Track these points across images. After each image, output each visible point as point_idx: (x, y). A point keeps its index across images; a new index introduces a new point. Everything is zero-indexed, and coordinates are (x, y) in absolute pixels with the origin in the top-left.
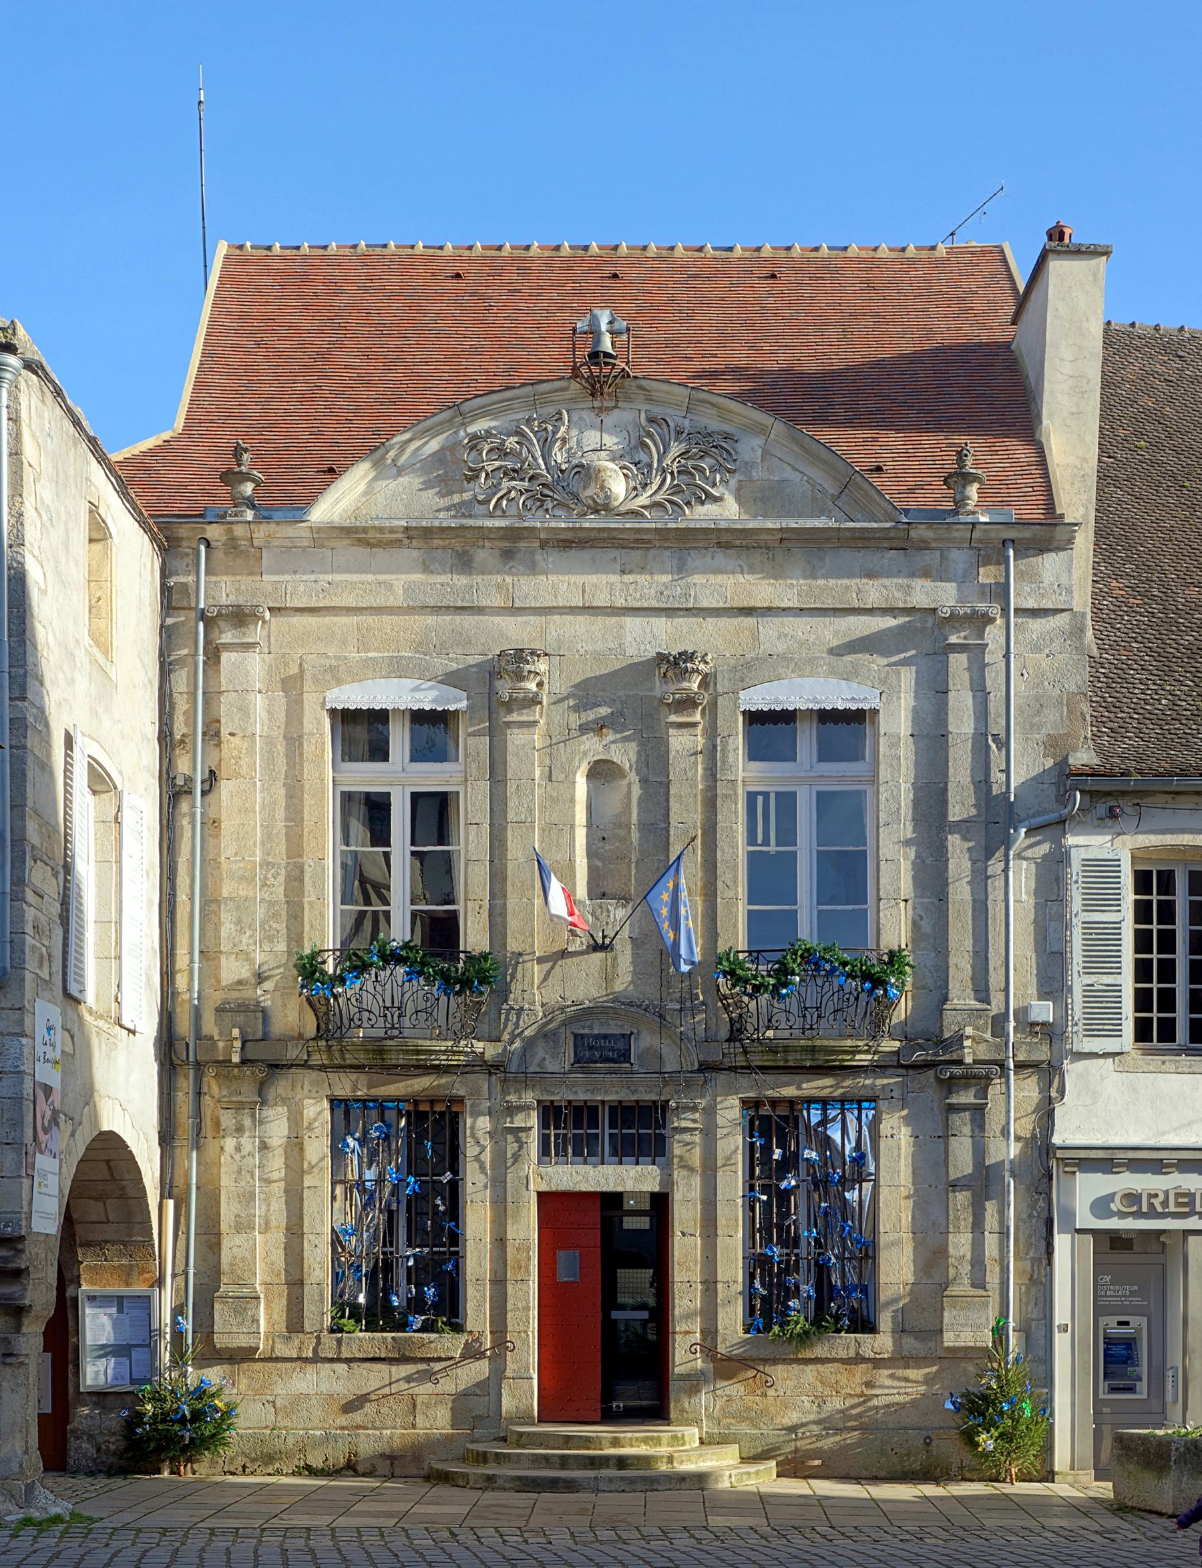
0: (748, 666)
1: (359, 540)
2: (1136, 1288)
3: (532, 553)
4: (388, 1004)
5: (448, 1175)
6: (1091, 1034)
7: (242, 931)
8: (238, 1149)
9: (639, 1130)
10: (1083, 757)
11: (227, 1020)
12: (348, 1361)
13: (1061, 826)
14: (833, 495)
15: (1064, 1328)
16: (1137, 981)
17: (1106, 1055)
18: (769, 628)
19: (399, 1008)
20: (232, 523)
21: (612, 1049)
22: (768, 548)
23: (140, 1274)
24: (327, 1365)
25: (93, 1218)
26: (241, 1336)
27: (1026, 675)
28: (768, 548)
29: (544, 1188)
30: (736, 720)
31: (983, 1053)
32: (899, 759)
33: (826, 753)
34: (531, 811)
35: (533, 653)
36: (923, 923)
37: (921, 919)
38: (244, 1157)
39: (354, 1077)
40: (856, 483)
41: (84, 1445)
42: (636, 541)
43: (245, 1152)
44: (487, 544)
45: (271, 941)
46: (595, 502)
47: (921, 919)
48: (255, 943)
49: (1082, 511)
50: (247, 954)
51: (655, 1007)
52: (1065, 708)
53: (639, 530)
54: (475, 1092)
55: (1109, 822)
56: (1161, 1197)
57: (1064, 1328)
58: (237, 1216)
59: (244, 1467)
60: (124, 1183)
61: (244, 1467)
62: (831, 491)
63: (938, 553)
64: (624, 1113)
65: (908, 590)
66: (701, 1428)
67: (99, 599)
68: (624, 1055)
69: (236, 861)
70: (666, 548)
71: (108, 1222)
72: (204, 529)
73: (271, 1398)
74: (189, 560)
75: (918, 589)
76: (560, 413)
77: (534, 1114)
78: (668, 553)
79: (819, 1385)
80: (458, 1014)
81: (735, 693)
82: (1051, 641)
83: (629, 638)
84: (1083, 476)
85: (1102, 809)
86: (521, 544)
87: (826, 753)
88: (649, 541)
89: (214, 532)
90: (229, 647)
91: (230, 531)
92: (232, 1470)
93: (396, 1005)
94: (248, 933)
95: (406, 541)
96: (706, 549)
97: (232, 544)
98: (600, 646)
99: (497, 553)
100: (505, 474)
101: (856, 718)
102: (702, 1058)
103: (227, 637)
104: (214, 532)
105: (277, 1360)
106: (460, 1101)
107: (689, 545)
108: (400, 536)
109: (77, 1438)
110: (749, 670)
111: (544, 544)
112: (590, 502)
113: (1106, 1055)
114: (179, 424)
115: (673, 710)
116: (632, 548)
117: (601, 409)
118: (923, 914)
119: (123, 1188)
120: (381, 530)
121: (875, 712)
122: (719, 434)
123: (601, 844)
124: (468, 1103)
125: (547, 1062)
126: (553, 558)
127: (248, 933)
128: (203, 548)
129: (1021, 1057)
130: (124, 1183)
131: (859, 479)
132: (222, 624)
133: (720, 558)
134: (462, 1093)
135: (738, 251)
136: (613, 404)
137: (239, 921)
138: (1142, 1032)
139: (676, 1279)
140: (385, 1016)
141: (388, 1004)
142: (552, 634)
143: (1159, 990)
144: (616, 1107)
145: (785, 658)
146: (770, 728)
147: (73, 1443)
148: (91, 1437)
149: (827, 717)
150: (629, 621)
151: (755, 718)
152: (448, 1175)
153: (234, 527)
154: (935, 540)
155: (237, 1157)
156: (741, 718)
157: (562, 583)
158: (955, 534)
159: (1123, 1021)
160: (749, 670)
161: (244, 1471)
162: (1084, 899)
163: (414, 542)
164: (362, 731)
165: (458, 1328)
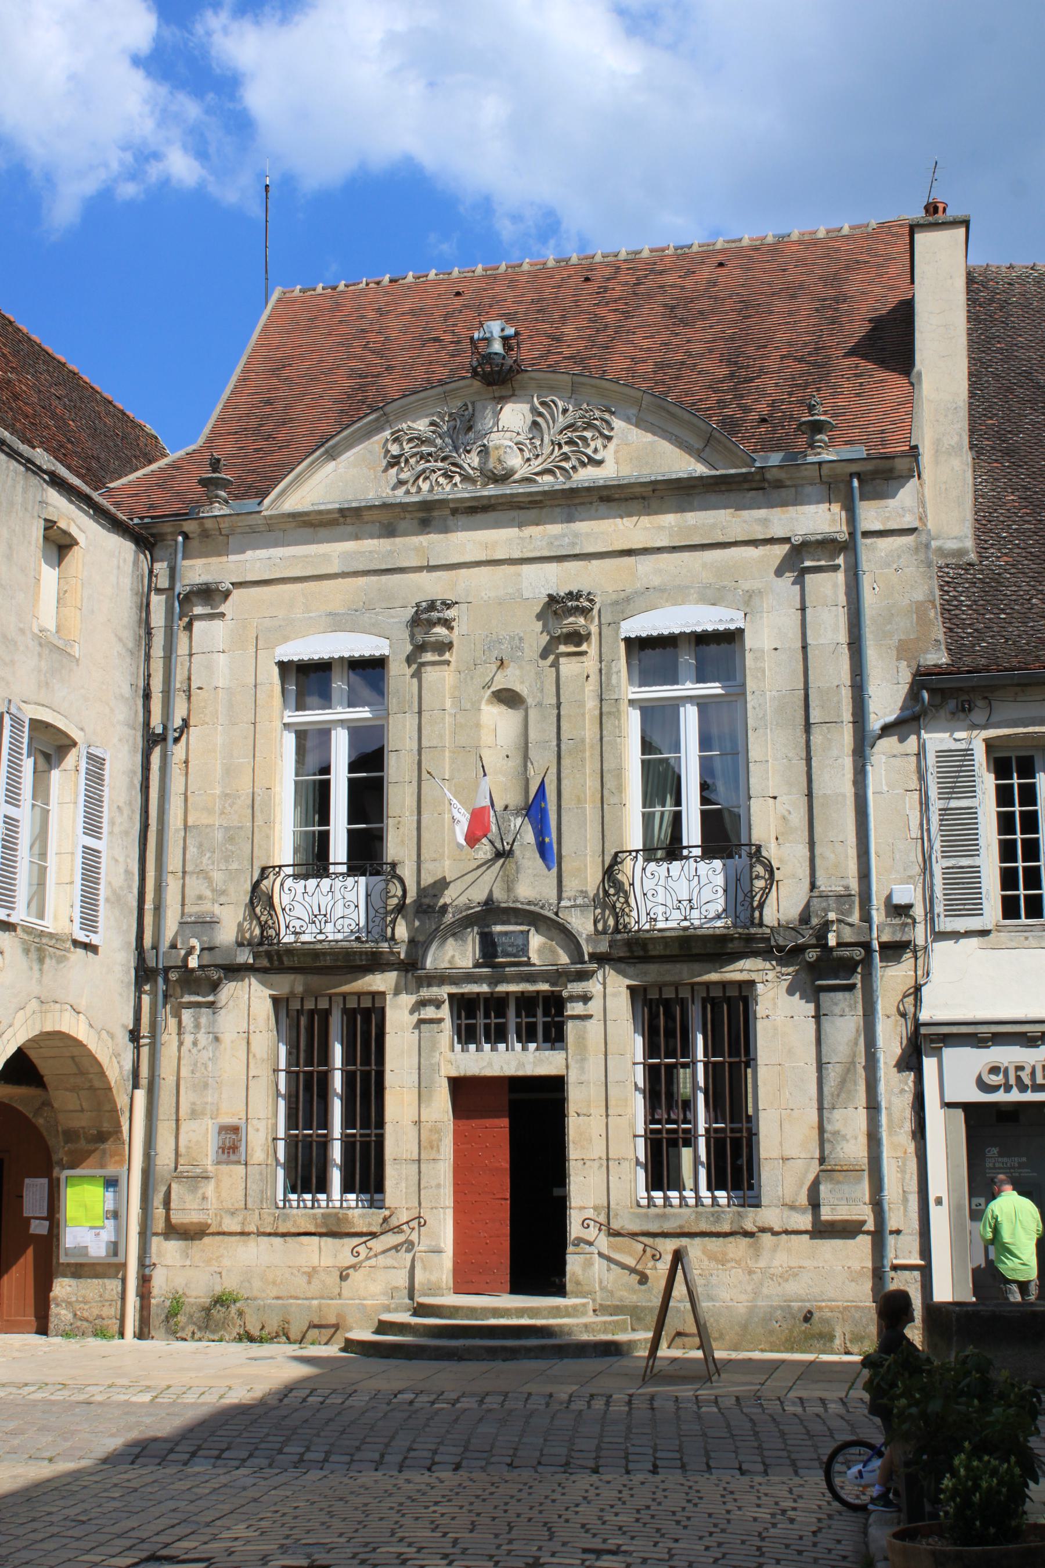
0: (628, 600)
1: (304, 522)
2: (1024, 1159)
3: (445, 520)
4: (316, 912)
6: (952, 912)
7: (202, 854)
8: (195, 1043)
9: (545, 1018)
10: (940, 657)
11: (187, 932)
13: (915, 723)
14: (698, 449)
15: (939, 1201)
16: (1002, 861)
17: (968, 934)
18: (645, 565)
19: (325, 916)
20: (203, 518)
21: (512, 945)
22: (644, 498)
23: (111, 1156)
24: (266, 1239)
25: (71, 1107)
26: (193, 1212)
27: (877, 589)
28: (644, 498)
29: (454, 1073)
30: (618, 646)
31: (848, 935)
32: (764, 671)
34: (441, 737)
35: (444, 603)
36: (790, 817)
37: (790, 813)
38: (199, 1051)
39: (292, 977)
40: (716, 438)
41: (63, 1312)
42: (530, 502)
43: (200, 1046)
44: (408, 516)
45: (227, 861)
46: (494, 474)
47: (790, 813)
48: (213, 864)
49: (956, 438)
50: (207, 873)
52: (915, 616)
53: (530, 494)
55: (962, 715)
56: (1028, 1070)
57: (939, 1201)
58: (194, 1104)
59: (193, 1333)
60: (91, 1076)
61: (193, 1333)
62: (697, 446)
63: (793, 490)
64: (526, 1003)
65: (765, 522)
66: (594, 1300)
67: (66, 591)
68: (523, 949)
69: (199, 795)
70: (556, 506)
71: (82, 1110)
72: (181, 525)
73: (218, 1270)
74: (171, 550)
75: (775, 521)
77: (446, 1006)
78: (558, 510)
79: (706, 1259)
80: (377, 920)
81: (617, 623)
82: (899, 557)
84: (956, 409)
85: (952, 704)
86: (436, 513)
88: (541, 501)
89: (190, 526)
91: (202, 525)
92: (184, 1336)
93: (323, 912)
94: (208, 855)
95: (342, 520)
96: (591, 503)
97: (205, 534)
99: (416, 522)
100: (421, 458)
101: (731, 638)
102: (591, 951)
103: (198, 610)
104: (190, 526)
105: (224, 1234)
107: (573, 502)
108: (337, 515)
109: (58, 1305)
110: (626, 604)
111: (455, 512)
112: (490, 474)
113: (968, 934)
114: (201, 441)
115: (562, 640)
116: (528, 508)
119: (90, 1081)
120: (320, 512)
121: (740, 631)
125: (457, 959)
126: (462, 520)
127: (208, 855)
128: (180, 539)
129: (885, 938)
130: (91, 1076)
131: (717, 434)
132: (194, 599)
133: (603, 508)
134: (382, 989)
135: (695, 249)
136: (510, 393)
137: (201, 845)
138: (1010, 909)
139: (571, 1157)
140: (314, 922)
141: (316, 912)
143: (1024, 868)
144: (549, 997)
145: (661, 590)
146: (653, 653)
147: (54, 1309)
148: (69, 1304)
149: (702, 639)
150: (526, 568)
151: (638, 646)
153: (205, 521)
154: (789, 479)
155: (194, 1051)
156: (622, 645)
157: (468, 542)
158: (806, 473)
159: (984, 901)
160: (626, 604)
161: (193, 1337)
162: (939, 788)
163: (349, 520)
164: (307, 679)
165: (376, 1204)
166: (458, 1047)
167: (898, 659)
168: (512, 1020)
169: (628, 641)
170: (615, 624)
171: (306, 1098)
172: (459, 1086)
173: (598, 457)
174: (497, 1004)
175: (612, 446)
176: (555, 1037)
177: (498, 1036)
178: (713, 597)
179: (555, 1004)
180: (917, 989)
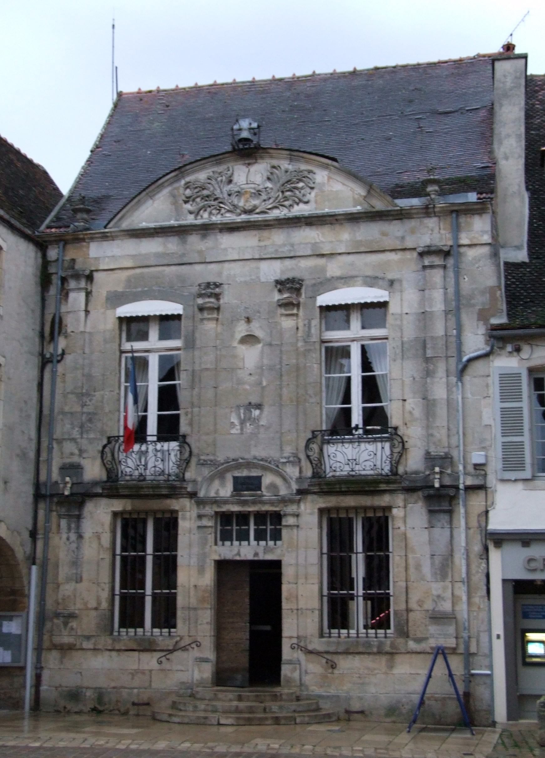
5: (528, 89)
7: (73, 428)
8: (68, 539)
9: (270, 524)
12: (119, 650)
33: (163, 336)
36: (414, 412)
47: (413, 409)
51: (274, 461)
54: (183, 509)
64: (261, 517)
76: (228, 168)
83: (262, 274)
87: (163, 336)
90: (73, 290)
98: (248, 279)
100: (202, 199)
106: (177, 512)
117: (249, 164)
118: (414, 407)
122: (306, 171)
123: (249, 377)
124: (180, 514)
142: (225, 273)
152: (528, 89)
166: (220, 543)
167: (479, 320)
168: (252, 527)
169: (321, 307)
170: (313, 298)
171: (131, 571)
172: (222, 566)
173: (305, 199)
174: (243, 518)
175: (313, 193)
176: (277, 536)
177: (243, 536)
178: (371, 281)
179: (277, 518)
180: (487, 512)
